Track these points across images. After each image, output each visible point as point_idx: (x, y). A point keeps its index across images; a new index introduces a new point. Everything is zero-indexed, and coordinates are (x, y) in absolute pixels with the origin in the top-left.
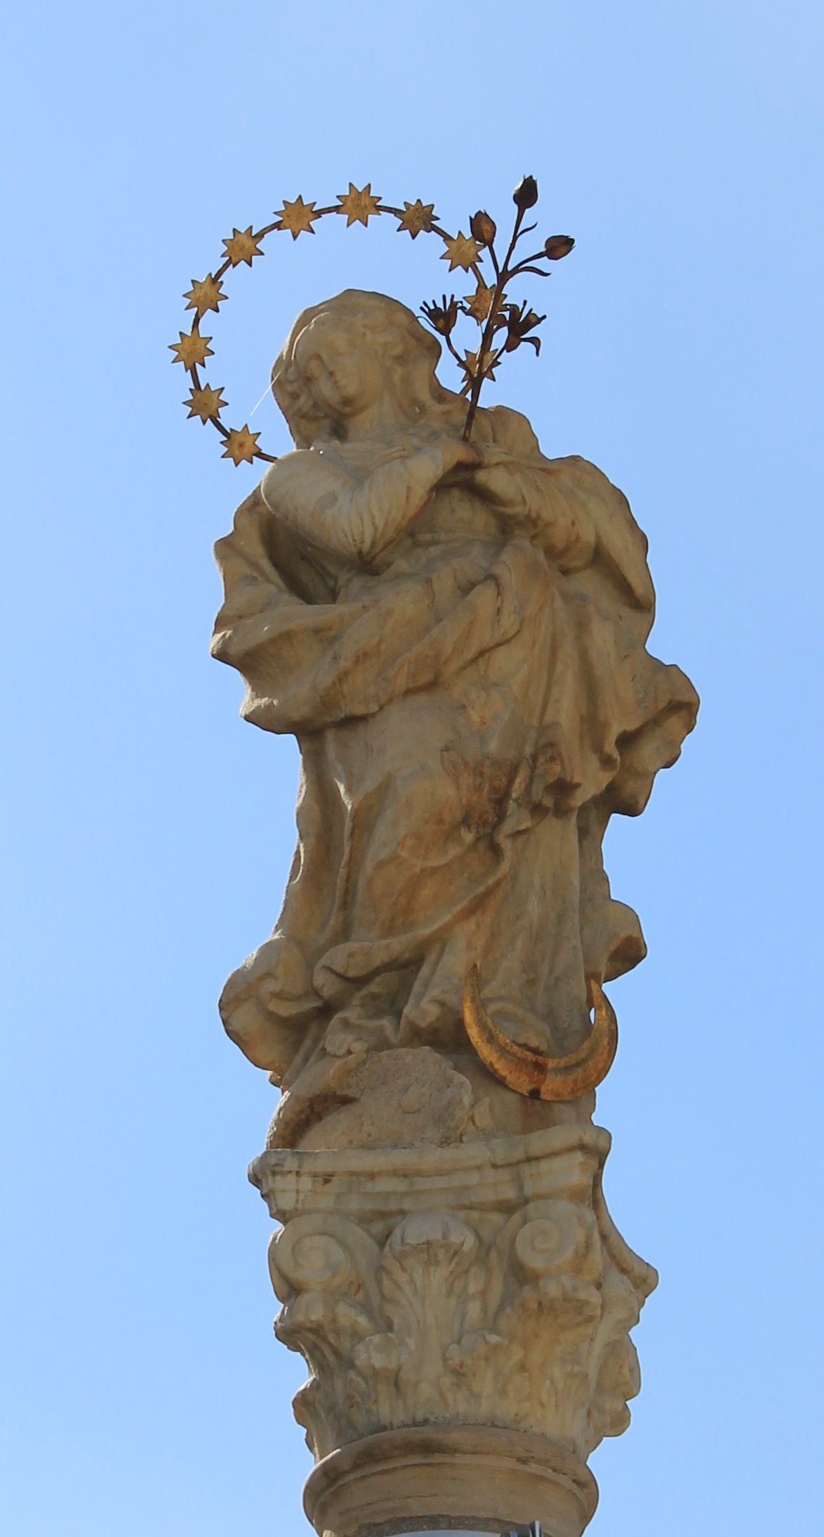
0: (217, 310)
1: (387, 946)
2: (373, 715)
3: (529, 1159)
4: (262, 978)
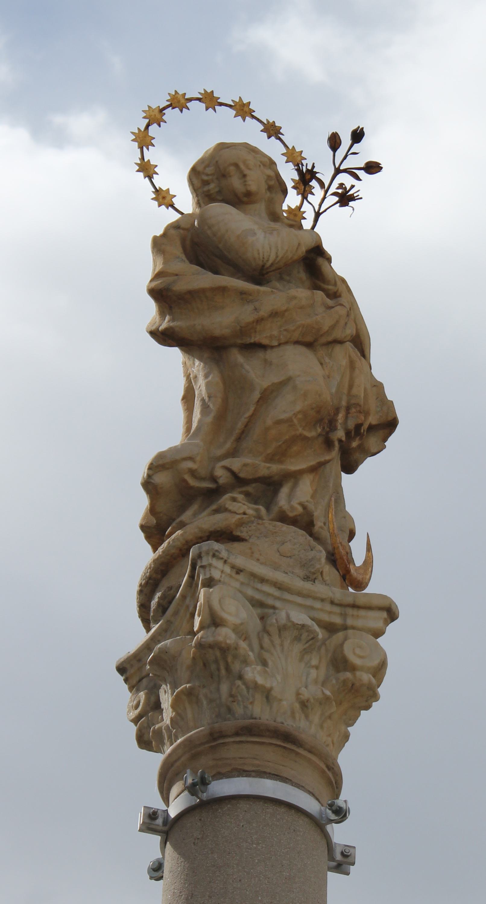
0: (160, 126)
1: (269, 468)
2: (272, 347)
3: (354, 606)
4: (185, 459)
